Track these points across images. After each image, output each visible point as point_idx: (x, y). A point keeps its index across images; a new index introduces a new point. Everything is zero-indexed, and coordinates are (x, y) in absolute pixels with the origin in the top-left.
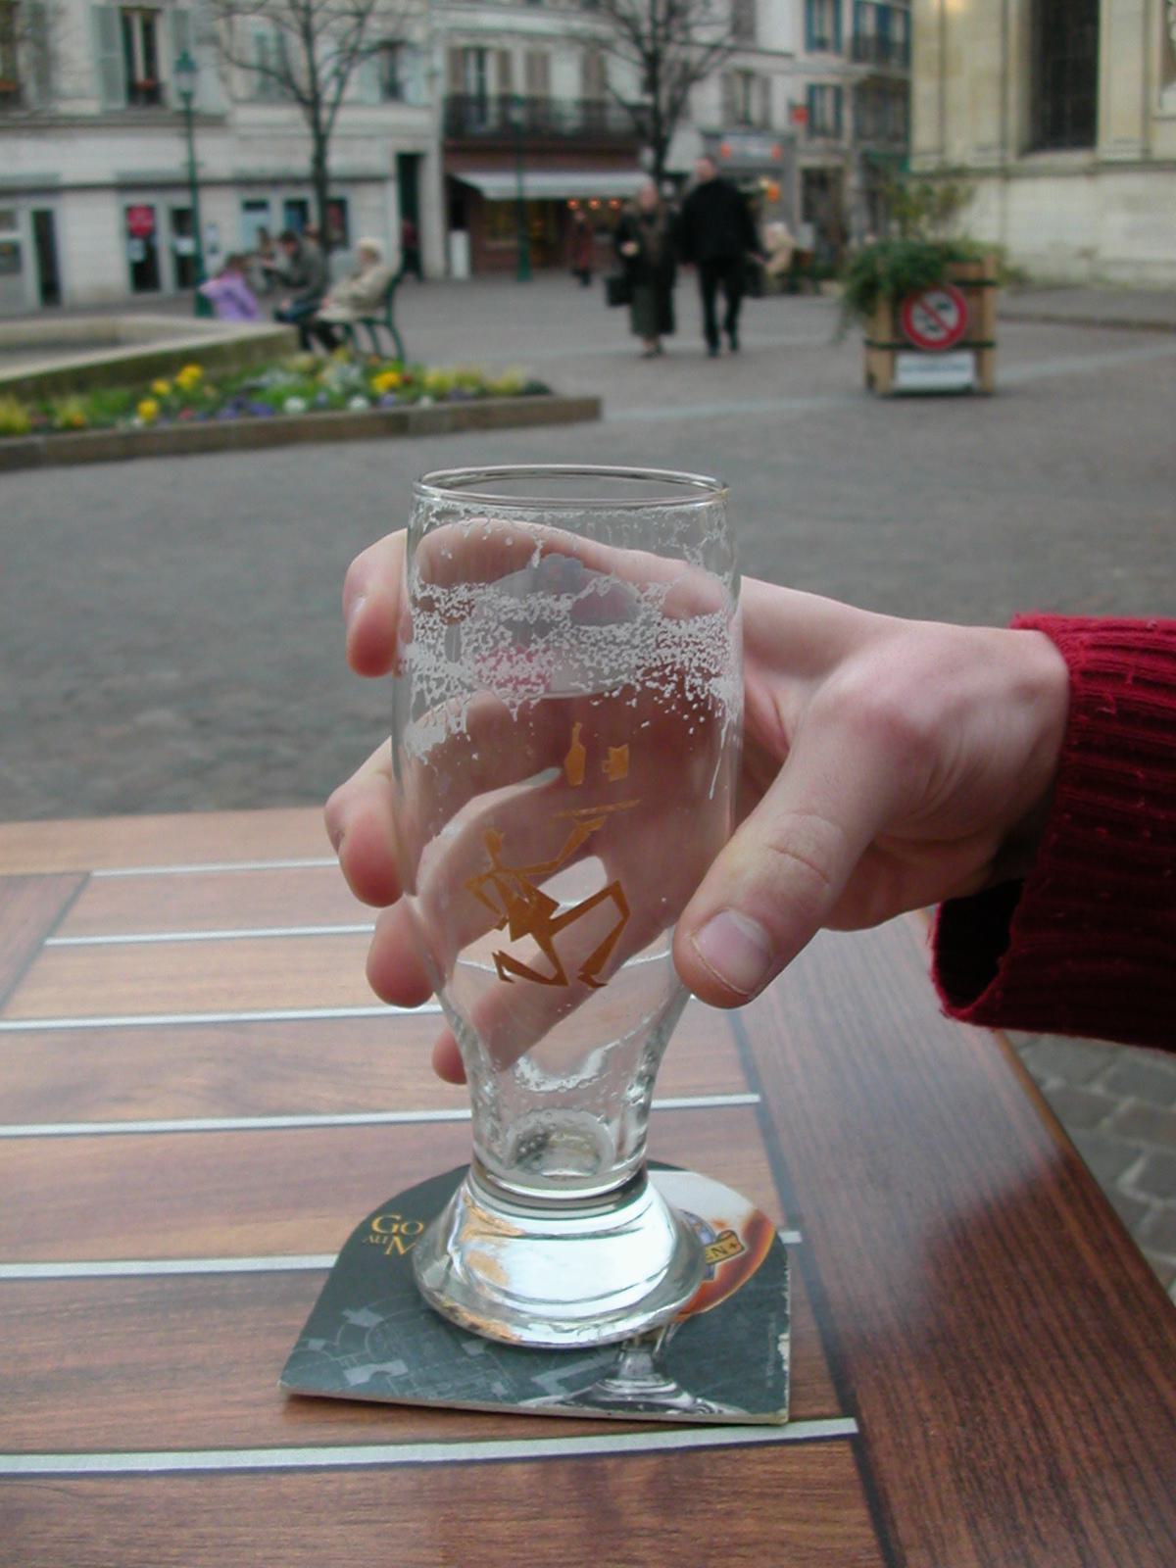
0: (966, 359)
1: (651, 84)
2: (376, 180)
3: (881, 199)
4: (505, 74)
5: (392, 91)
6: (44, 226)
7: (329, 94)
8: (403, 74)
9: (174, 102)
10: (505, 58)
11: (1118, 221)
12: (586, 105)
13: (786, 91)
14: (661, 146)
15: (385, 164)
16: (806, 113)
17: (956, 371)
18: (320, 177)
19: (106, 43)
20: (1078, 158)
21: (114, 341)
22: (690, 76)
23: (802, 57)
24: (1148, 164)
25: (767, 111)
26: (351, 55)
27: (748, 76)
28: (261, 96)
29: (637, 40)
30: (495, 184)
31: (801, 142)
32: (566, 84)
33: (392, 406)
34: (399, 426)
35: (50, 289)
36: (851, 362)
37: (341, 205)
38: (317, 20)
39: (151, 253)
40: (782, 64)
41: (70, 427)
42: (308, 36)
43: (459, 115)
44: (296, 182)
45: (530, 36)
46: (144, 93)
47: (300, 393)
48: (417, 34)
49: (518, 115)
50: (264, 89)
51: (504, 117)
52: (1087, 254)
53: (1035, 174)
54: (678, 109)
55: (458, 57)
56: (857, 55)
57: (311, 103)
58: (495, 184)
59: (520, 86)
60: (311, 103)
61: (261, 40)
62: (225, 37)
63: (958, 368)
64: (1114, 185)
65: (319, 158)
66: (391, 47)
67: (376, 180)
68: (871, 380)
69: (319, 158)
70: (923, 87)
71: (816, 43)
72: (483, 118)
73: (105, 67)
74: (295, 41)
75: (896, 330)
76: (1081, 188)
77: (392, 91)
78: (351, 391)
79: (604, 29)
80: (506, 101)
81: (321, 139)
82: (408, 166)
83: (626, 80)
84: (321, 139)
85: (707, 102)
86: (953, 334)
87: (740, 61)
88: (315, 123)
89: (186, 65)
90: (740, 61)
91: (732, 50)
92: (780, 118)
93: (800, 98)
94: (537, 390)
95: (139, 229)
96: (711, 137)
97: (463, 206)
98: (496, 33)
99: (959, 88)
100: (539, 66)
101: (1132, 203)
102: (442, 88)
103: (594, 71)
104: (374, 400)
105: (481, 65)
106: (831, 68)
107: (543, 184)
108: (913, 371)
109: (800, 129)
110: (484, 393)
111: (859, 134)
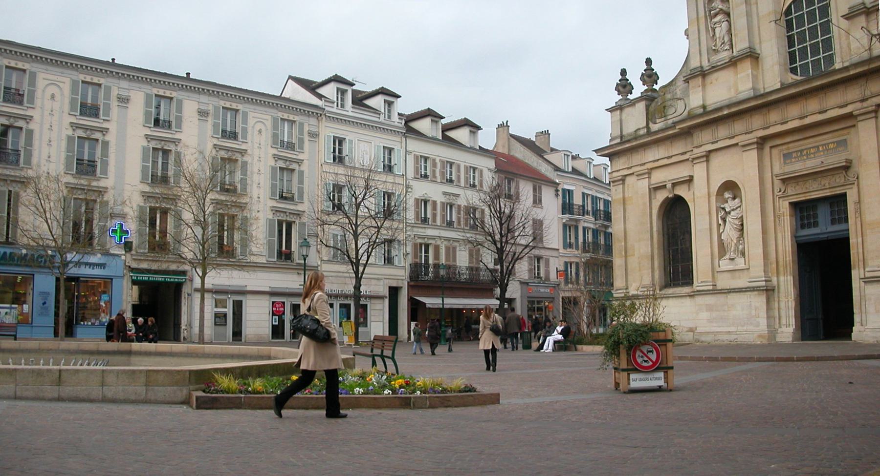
0: (661, 374)
1: (499, 261)
2: (381, 298)
3: (601, 312)
4: (437, 256)
5: (389, 261)
6: (238, 307)
7: (363, 261)
8: (393, 253)
9: (297, 259)
10: (437, 248)
11: (705, 315)
12: (470, 269)
13: (556, 264)
14: (504, 290)
15: (386, 293)
16: (564, 273)
17: (657, 380)
18: (357, 295)
19: (271, 234)
20: (686, 290)
21: (269, 358)
22: (516, 259)
23: (562, 251)
24: (715, 291)
25: (547, 273)
26: (373, 245)
27: (539, 258)
28: (333, 260)
29: (494, 242)
30: (432, 302)
31: (562, 285)
32: (463, 260)
33: (403, 393)
34: (406, 404)
35: (237, 334)
36: (608, 378)
37: (365, 307)
38: (359, 230)
39: (282, 322)
40: (555, 253)
41: (255, 392)
42: (356, 236)
43: (417, 272)
44: (346, 297)
45: (448, 239)
46: (285, 256)
47: (360, 386)
48: (401, 237)
49: (442, 272)
50: (335, 256)
51: (436, 273)
52: (691, 330)
53: (667, 297)
54: (510, 272)
55: (417, 247)
56: (585, 250)
57: (356, 264)
58: (432, 302)
59: (443, 260)
60: (356, 264)
61: (335, 236)
62: (320, 234)
63: (659, 379)
64: (700, 300)
65: (357, 287)
66: (390, 242)
67: (381, 298)
68: (617, 385)
69: (357, 287)
70: (618, 262)
71: (568, 245)
72: (427, 274)
73: (270, 244)
74: (350, 237)
75: (629, 362)
76: (688, 301)
77: (389, 261)
78: (384, 387)
79: (480, 238)
80: (437, 266)
81: (358, 279)
82: (394, 292)
83: (488, 258)
84: (358, 279)
85: (522, 269)
86: (654, 363)
87: (536, 252)
88: (356, 273)
89: (305, 244)
90: (536, 252)
91: (534, 248)
92: (553, 276)
93: (562, 268)
94: (470, 389)
95: (277, 312)
96: (523, 283)
97: (416, 310)
98: (433, 238)
99: (633, 262)
100: (451, 252)
101: (710, 308)
102: (410, 259)
103: (474, 255)
104: (394, 391)
105: (427, 251)
106: (575, 255)
107: (452, 302)
108: (637, 381)
109: (562, 279)
110: (444, 391)
111: (587, 284)
